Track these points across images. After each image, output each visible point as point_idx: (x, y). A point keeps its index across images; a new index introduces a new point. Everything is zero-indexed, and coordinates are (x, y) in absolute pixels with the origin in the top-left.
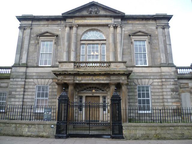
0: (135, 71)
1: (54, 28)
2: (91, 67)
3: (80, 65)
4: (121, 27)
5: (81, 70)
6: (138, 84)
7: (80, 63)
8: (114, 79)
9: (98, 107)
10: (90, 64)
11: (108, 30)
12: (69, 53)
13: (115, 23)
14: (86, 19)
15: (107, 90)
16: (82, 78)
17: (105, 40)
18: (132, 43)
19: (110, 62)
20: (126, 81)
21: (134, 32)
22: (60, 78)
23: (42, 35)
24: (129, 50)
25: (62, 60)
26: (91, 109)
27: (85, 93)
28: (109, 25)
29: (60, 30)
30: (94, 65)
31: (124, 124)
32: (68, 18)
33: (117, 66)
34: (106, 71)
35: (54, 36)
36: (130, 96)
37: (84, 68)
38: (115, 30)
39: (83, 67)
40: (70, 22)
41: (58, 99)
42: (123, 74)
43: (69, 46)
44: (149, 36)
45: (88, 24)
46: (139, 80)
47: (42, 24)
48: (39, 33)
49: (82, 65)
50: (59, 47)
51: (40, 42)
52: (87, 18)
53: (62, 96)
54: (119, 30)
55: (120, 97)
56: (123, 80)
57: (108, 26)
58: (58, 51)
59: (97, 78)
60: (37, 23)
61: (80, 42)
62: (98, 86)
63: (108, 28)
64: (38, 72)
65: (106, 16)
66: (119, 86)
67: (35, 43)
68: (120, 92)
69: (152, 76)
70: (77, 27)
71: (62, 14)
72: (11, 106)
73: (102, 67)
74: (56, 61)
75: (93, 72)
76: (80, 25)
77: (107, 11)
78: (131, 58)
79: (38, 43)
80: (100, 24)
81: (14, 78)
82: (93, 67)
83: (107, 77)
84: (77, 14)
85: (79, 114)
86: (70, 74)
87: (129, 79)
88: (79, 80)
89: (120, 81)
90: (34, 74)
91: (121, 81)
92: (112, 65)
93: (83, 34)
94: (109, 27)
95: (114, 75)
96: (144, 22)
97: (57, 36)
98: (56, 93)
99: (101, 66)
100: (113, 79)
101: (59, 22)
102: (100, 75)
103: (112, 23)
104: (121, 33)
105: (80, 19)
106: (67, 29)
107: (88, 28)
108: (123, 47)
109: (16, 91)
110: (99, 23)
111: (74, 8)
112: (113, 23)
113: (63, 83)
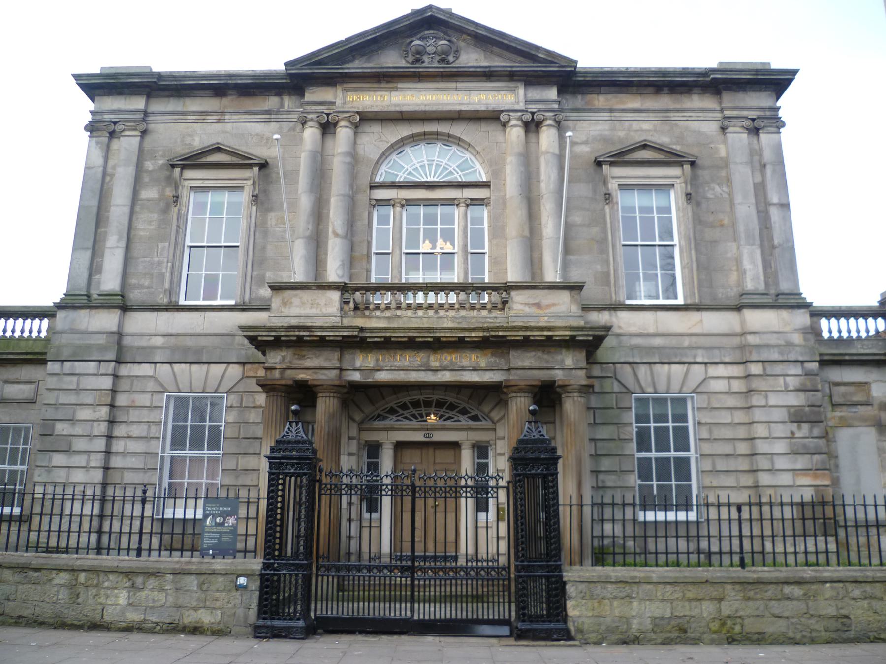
1: (248, 130)
3: (368, 302)
6: (638, 389)
8: (526, 364)
9: (455, 492)
13: (533, 108)
15: (495, 415)
16: (377, 360)
17: (486, 185)
18: (608, 197)
19: (508, 288)
20: (582, 373)
21: (617, 147)
22: (275, 358)
23: (193, 161)
24: (595, 230)
25: (285, 277)
28: (503, 117)
29: (276, 136)
30: (432, 298)
31: (570, 574)
32: (312, 85)
34: (487, 329)
35: (250, 166)
36: (599, 444)
37: (388, 314)
38: (532, 136)
39: (383, 306)
42: (570, 343)
44: (687, 167)
45: (404, 109)
46: (643, 371)
47: (194, 113)
48: (182, 150)
49: (377, 299)
50: (272, 217)
51: (184, 192)
52: (400, 85)
54: (547, 137)
56: (566, 367)
57: (499, 118)
58: (265, 233)
60: (172, 105)
61: (371, 194)
63: (500, 128)
64: (174, 332)
65: (488, 75)
66: (547, 396)
67: (162, 196)
68: (554, 423)
69: (700, 352)
70: (356, 127)
71: (286, 65)
72: (50, 490)
73: (473, 308)
75: (429, 330)
77: (492, 52)
79: (176, 199)
80: (460, 112)
81: (63, 361)
82: (430, 307)
83: (493, 354)
84: (357, 65)
86: (322, 343)
88: (363, 367)
90: (159, 341)
91: (558, 375)
93: (384, 155)
94: (504, 125)
95: (526, 344)
96: (665, 101)
97: (263, 165)
98: (259, 431)
99: (467, 306)
100: (520, 364)
101: (272, 102)
102: (459, 344)
103: (517, 107)
104: (557, 152)
105: (369, 90)
106: (311, 133)
107: (405, 131)
108: (566, 217)
109: (72, 421)
110: (457, 108)
111: (343, 38)
112: (521, 106)
113: (290, 382)
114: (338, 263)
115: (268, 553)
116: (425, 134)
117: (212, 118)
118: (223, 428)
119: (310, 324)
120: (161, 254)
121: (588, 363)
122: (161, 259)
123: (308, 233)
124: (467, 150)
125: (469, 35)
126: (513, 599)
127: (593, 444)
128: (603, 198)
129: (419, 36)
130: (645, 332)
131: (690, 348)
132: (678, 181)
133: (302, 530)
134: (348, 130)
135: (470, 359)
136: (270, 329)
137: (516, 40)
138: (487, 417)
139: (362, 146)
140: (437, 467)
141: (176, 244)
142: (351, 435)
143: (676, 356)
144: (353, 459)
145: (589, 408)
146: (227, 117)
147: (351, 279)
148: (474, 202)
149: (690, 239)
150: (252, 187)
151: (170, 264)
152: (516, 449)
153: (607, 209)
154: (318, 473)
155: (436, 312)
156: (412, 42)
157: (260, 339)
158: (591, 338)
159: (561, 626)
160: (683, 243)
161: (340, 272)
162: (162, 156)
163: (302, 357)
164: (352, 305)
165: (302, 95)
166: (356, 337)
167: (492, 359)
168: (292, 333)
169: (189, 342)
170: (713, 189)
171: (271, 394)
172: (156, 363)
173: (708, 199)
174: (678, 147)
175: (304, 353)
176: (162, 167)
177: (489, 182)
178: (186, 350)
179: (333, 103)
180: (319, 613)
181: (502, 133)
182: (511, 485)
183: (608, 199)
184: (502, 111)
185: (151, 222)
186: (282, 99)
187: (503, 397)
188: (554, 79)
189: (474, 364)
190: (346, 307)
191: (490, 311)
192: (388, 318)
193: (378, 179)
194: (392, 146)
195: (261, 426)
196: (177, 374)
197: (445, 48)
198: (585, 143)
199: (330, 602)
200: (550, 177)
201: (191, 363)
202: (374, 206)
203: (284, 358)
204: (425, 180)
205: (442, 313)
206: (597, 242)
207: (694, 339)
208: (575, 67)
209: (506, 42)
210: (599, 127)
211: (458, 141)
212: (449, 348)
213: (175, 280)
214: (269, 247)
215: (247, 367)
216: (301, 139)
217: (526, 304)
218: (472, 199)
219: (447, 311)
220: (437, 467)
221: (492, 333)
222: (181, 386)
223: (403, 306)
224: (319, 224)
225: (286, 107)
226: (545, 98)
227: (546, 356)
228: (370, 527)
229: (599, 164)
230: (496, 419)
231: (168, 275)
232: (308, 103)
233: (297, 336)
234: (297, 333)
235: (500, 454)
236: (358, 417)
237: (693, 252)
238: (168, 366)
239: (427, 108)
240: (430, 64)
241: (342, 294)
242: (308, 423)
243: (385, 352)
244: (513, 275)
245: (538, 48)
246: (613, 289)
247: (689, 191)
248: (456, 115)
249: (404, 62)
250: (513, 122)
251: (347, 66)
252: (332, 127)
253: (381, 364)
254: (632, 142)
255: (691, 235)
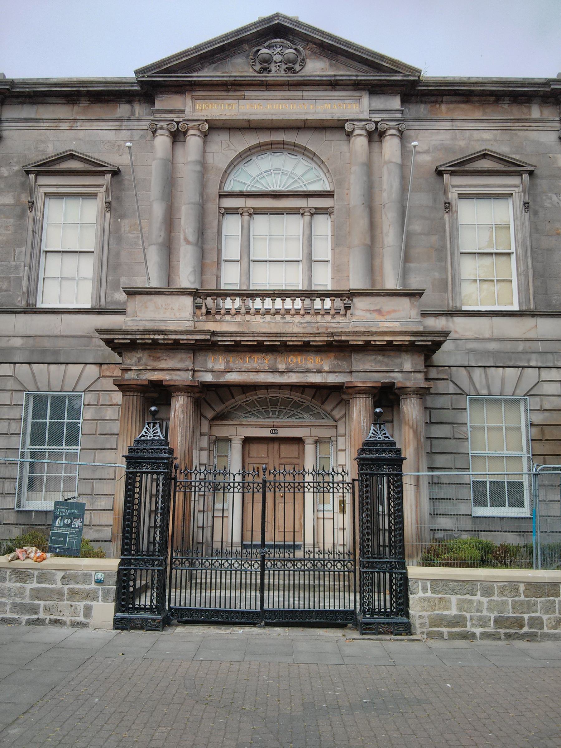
0: (458, 329)
1: (100, 137)
2: (268, 312)
3: (218, 306)
4: (401, 134)
5: (225, 326)
6: (473, 392)
7: (219, 295)
8: (367, 367)
9: (299, 487)
10: (263, 300)
11: (345, 148)
12: (169, 249)
13: (377, 117)
14: (244, 98)
15: (337, 414)
16: (228, 362)
17: (329, 195)
18: (448, 206)
19: (351, 294)
20: (420, 376)
21: (458, 157)
22: (132, 360)
23: (46, 168)
24: (434, 239)
25: (140, 283)
26: (269, 496)
27: (242, 426)
28: (348, 127)
29: (128, 144)
30: (278, 304)
31: (415, 571)
32: (162, 93)
33: (379, 311)
34: (332, 334)
35: (103, 173)
36: (435, 442)
37: (238, 318)
38: (376, 145)
39: (233, 311)
40: (171, 112)
41: (127, 458)
42: (410, 348)
43: (170, 222)
44: (526, 177)
46: (477, 373)
48: (36, 157)
49: (228, 304)
50: (125, 224)
51: (39, 199)
52: (247, 94)
53: (143, 442)
54: (391, 146)
55: (399, 450)
56: (405, 371)
57: (343, 128)
58: (119, 239)
59: (295, 360)
60: (27, 112)
61: (222, 202)
62: (296, 396)
63: (344, 137)
64: (32, 333)
65: (333, 84)
66: (386, 399)
67: (18, 201)
68: (392, 421)
69: (534, 356)
70: (205, 135)
71: (136, 72)
73: (317, 312)
74: (116, 286)
75: (276, 334)
76: (219, 124)
78: (444, 277)
79: (32, 204)
80: (305, 121)
82: (278, 312)
83: (336, 358)
84: (207, 74)
85: (218, 514)
86: (175, 346)
87: (431, 368)
88: (216, 369)
89: (392, 375)
90: (18, 342)
91: (398, 378)
92: (359, 303)
93: (233, 165)
94: (349, 135)
95: (367, 348)
96: (508, 111)
97: (116, 173)
98: (115, 427)
99: (312, 312)
100: (361, 367)
101: (123, 110)
102: (305, 348)
103: (361, 117)
104: (399, 161)
105: (217, 98)
106: (162, 141)
107: (252, 140)
108: (408, 226)
110: (303, 117)
112: (365, 116)
113: (147, 383)
114: (190, 269)
115: (125, 550)
116: (271, 143)
117: (64, 125)
118: (80, 425)
119: (164, 328)
120: (18, 259)
121: (426, 366)
122: (18, 263)
123: (160, 240)
124: (312, 159)
125: (315, 44)
126: (358, 588)
127: (429, 442)
128: (442, 206)
129: (265, 45)
130: (481, 337)
131: (525, 352)
132: (516, 190)
133: (158, 520)
134: (197, 138)
135: (315, 362)
136: (126, 332)
137: (361, 49)
138: (329, 415)
139: (211, 154)
140: (283, 461)
141: (32, 248)
142: (203, 431)
143: (510, 360)
144: (204, 454)
145: (426, 408)
146: (79, 124)
147: (202, 286)
148: (318, 211)
149: (527, 247)
150: (105, 194)
151: (26, 268)
152: (362, 451)
153: (447, 217)
154: (174, 470)
155: (283, 317)
156: (260, 50)
157: (116, 341)
158: (430, 343)
159: (405, 620)
160: (520, 251)
161: (192, 279)
162: (17, 163)
163: (157, 359)
164: (204, 310)
165: (153, 103)
166: (208, 340)
167: (335, 362)
168: (147, 336)
169: (47, 344)
170: (551, 199)
171: (128, 393)
172: (15, 363)
173: (545, 208)
174: (517, 157)
175: (159, 355)
176: (17, 173)
177: (333, 191)
178: (44, 351)
179: (183, 112)
180: (172, 605)
181: (346, 142)
182: (356, 483)
183: (448, 208)
184: (347, 120)
185: (7, 227)
186: (132, 107)
187: (344, 397)
188: (398, 89)
189: (318, 367)
190: (198, 311)
191: (333, 316)
192: (238, 322)
193: (229, 187)
194: (240, 155)
195: (118, 423)
196: (36, 373)
197: (292, 57)
198: (427, 152)
199: (183, 591)
200: (392, 186)
201: (49, 363)
202: (223, 214)
203: (139, 359)
204: (272, 189)
205: (288, 318)
206: (436, 250)
207: (528, 344)
208: (419, 77)
209: (351, 51)
210: (440, 137)
211: (303, 151)
212: (295, 351)
213: (32, 283)
214: (123, 253)
215: (104, 367)
216: (152, 146)
217: (367, 310)
218: (316, 208)
219: (293, 316)
220: (283, 461)
221: (336, 338)
222: (39, 385)
223: (252, 311)
224: (170, 232)
225: (137, 115)
226: (389, 107)
227: (386, 360)
228: (223, 517)
229: (440, 173)
230: (337, 417)
231: (25, 279)
232: (158, 111)
233: (152, 339)
234: (152, 337)
235: (341, 450)
236: (210, 414)
237: (529, 260)
238: (27, 365)
239: (274, 117)
240: (277, 73)
241: (194, 299)
242: (163, 420)
243: (235, 354)
244: (356, 282)
245: (382, 57)
246: (450, 295)
247: (527, 200)
248: (302, 125)
249: (251, 70)
250: (356, 132)
251: (196, 74)
252: (182, 137)
253: (232, 365)
254: (473, 152)
255: (528, 244)
